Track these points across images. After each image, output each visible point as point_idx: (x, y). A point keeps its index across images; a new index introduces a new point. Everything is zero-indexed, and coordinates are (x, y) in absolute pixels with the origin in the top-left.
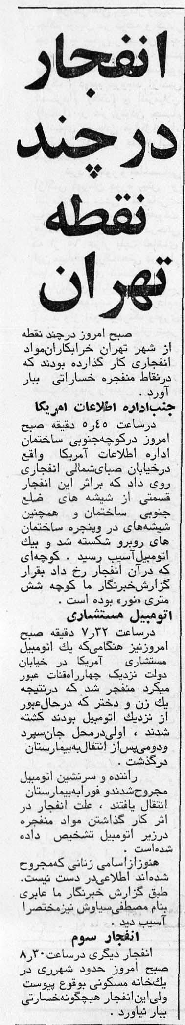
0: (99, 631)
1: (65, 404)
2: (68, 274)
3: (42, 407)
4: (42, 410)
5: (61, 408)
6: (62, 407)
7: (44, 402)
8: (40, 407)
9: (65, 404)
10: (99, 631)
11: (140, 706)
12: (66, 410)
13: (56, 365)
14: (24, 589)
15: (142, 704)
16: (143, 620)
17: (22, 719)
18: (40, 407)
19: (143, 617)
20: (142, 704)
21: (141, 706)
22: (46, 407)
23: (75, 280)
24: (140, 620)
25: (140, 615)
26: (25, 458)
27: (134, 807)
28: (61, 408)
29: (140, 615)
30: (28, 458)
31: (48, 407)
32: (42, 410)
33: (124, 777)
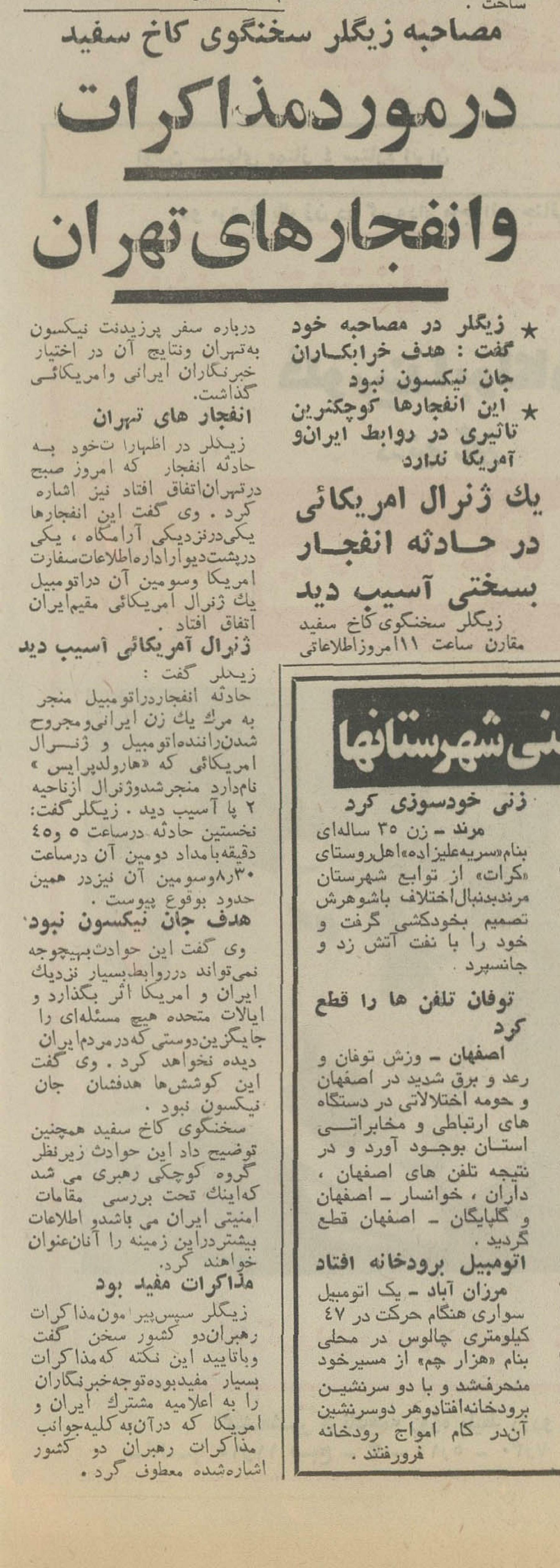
0: (383, 827)
1: (401, 489)
2: (65, 225)
3: (346, 502)
4: (347, 507)
5: (391, 501)
6: (395, 500)
7: (350, 489)
8: (340, 502)
9: (401, 489)
10: (383, 827)
11: (413, 834)
12: (403, 506)
13: (441, 922)
14: (322, 904)
15: (417, 831)
16: (480, 1269)
17: (322, 1433)
18: (340, 502)
19: (481, 1265)
20: (417, 831)
21: (415, 834)
22: (355, 502)
23: (74, 232)
24: (476, 1270)
25: (477, 1262)
26: (323, 1225)
27: (388, 900)
28: (391, 501)
29: (477, 1262)
30: (327, 1225)
31: (360, 499)
32: (347, 507)
33: (386, 944)
